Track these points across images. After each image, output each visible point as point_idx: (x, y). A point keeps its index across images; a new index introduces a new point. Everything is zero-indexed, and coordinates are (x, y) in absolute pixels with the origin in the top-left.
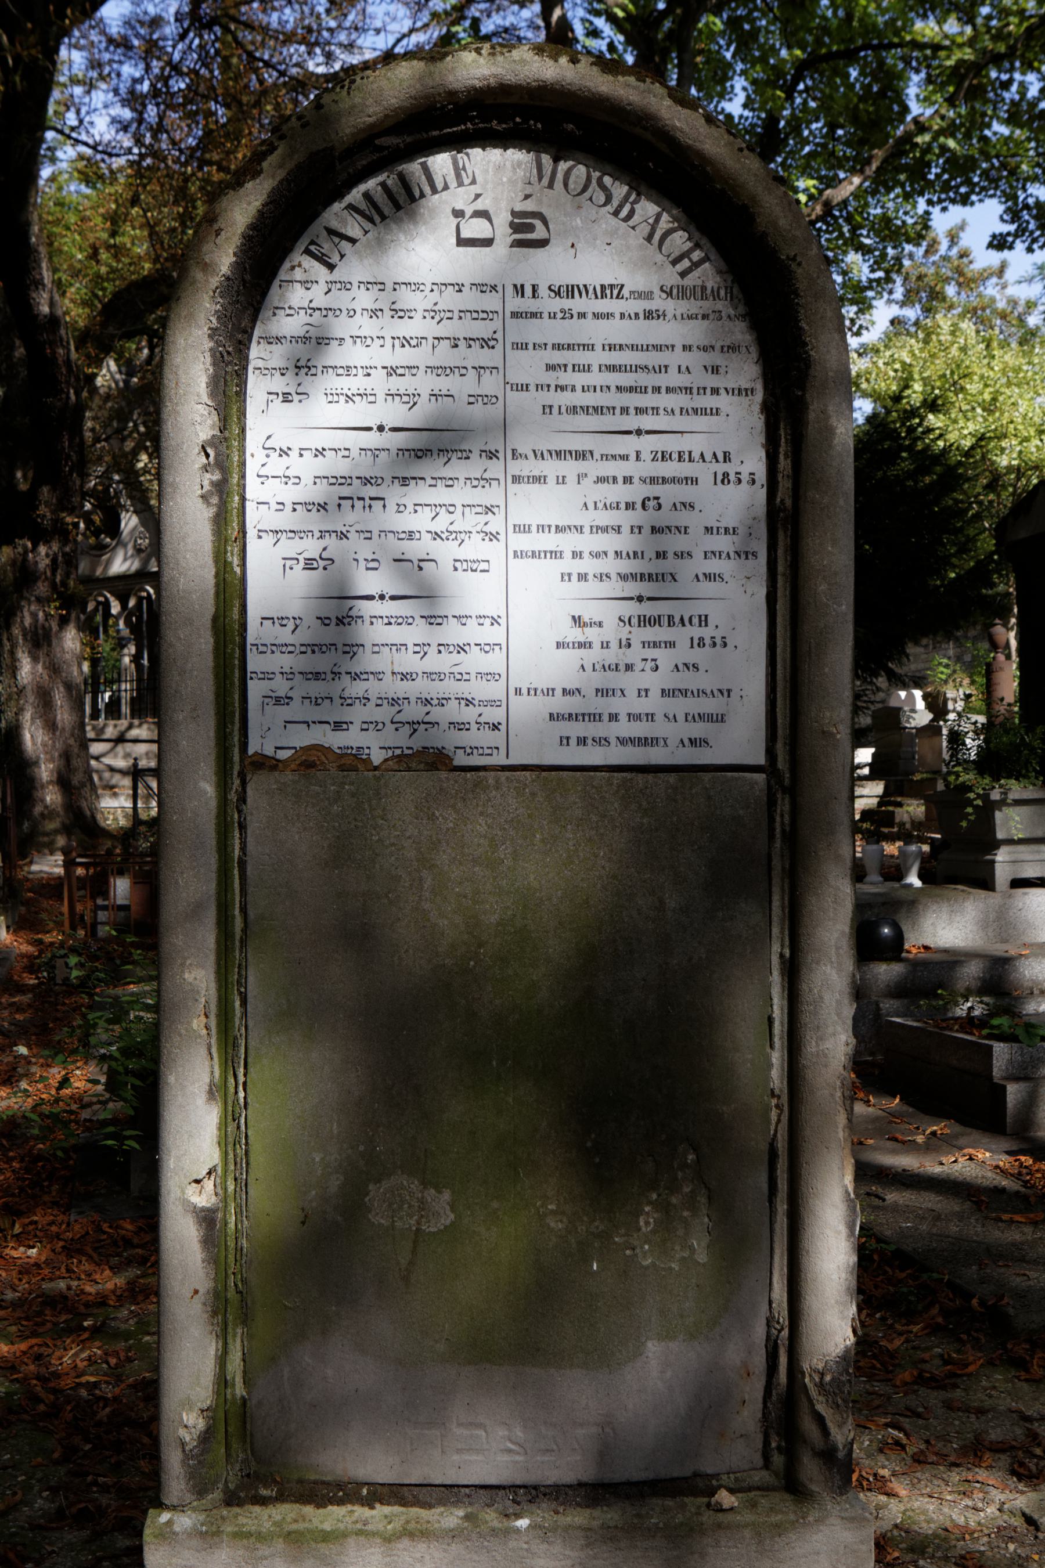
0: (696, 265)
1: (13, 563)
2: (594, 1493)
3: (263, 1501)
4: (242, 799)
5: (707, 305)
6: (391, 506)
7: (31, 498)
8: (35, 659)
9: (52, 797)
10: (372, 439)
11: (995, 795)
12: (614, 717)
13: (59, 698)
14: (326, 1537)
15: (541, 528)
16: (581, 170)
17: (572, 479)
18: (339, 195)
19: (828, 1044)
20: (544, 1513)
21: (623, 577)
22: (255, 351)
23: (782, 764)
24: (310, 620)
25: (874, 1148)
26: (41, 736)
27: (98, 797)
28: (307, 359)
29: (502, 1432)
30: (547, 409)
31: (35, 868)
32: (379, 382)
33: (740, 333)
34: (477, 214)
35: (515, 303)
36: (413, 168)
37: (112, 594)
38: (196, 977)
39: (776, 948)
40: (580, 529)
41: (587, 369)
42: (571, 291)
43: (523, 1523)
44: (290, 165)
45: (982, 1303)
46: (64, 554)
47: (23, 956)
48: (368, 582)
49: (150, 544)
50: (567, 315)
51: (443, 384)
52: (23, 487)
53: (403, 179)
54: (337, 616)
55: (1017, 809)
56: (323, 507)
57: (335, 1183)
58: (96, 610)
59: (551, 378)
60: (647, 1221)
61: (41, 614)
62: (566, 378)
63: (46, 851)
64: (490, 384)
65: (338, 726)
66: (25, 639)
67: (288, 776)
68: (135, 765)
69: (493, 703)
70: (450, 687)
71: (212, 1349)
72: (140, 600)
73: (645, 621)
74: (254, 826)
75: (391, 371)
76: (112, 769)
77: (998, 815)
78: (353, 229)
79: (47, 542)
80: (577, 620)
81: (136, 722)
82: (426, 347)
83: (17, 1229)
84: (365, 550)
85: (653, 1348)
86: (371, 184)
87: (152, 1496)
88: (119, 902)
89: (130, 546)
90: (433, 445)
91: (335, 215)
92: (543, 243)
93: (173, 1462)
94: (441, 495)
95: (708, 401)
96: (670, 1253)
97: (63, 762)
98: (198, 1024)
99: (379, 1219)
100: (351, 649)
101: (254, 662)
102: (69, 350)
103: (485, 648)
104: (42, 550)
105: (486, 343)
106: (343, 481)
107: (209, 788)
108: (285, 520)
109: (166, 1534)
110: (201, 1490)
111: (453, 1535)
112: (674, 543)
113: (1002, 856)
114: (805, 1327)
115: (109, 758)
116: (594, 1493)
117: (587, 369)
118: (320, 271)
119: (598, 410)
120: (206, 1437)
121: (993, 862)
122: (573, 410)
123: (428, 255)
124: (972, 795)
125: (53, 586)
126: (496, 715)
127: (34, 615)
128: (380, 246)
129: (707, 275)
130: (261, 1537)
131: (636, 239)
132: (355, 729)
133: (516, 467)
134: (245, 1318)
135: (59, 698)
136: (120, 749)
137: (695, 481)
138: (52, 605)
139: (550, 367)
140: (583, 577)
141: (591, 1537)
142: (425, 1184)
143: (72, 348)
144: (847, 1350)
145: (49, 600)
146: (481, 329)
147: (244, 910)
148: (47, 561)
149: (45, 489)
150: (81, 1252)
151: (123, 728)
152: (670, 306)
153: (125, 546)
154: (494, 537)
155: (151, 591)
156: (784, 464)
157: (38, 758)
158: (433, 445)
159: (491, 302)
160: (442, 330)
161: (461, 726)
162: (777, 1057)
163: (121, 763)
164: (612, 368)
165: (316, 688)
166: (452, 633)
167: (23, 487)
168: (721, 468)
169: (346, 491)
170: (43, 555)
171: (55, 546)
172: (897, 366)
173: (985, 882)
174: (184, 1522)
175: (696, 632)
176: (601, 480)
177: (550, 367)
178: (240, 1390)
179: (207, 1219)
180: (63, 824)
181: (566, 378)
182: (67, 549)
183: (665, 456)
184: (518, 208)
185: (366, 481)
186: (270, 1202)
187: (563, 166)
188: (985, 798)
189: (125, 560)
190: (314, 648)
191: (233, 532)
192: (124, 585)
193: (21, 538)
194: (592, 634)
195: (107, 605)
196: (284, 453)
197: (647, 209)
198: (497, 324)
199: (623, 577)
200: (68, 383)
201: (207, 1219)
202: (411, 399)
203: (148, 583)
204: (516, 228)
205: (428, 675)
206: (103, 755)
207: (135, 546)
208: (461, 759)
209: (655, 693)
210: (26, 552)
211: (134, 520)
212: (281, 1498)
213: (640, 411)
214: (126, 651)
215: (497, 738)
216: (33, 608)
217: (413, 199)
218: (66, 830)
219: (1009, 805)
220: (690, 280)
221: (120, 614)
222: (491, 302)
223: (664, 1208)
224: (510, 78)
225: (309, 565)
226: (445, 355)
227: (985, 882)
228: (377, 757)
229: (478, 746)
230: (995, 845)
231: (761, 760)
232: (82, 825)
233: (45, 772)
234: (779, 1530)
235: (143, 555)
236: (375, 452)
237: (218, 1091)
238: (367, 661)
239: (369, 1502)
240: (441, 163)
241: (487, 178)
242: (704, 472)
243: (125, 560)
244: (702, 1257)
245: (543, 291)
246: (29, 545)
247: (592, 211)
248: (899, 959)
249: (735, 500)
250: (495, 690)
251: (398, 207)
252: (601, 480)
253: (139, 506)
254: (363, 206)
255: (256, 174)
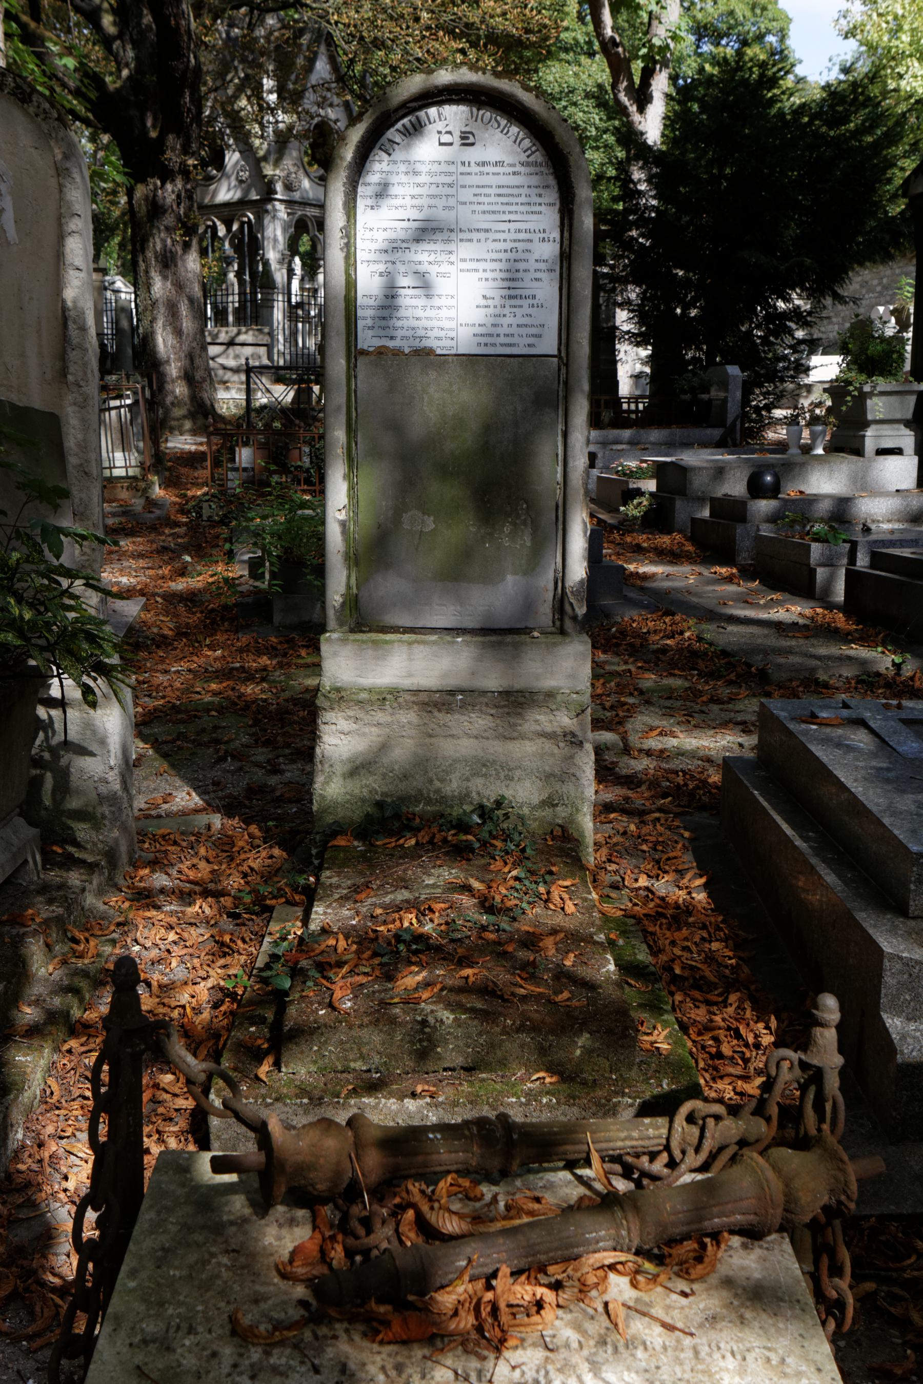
0: (533, 153)
1: (146, 198)
2: (484, 631)
3: (364, 632)
4: (356, 366)
5: (538, 169)
6: (413, 250)
7: (160, 145)
8: (165, 278)
9: (180, 390)
10: (405, 224)
11: (867, 388)
12: (498, 335)
13: (184, 309)
14: (386, 642)
15: (471, 260)
16: (488, 114)
17: (483, 240)
18: (392, 125)
19: (577, 463)
20: (468, 638)
21: (503, 280)
22: (360, 189)
23: (563, 354)
24: (381, 296)
25: (731, 607)
26: (171, 340)
27: (215, 390)
28: (382, 192)
29: (452, 608)
30: (474, 212)
31: (170, 445)
32: (408, 201)
33: (551, 181)
34: (447, 132)
35: (462, 169)
36: (422, 114)
37: (219, 219)
38: (339, 435)
39: (560, 427)
40: (486, 260)
41: (489, 195)
42: (484, 164)
43: (459, 639)
44: (374, 117)
45: (757, 669)
46: (187, 191)
47: (175, 504)
48: (403, 281)
49: (250, 176)
50: (482, 173)
51: (432, 202)
52: (153, 134)
53: (417, 118)
54: (389, 299)
55: (884, 398)
56: (386, 251)
57: (390, 513)
58: (206, 232)
59: (475, 199)
60: (507, 529)
61: (169, 241)
62: (481, 199)
63: (177, 433)
64: (452, 202)
65: (392, 338)
66: (157, 261)
67: (373, 358)
68: (247, 364)
69: (451, 329)
70: (435, 323)
71: (345, 573)
72: (242, 224)
73: (511, 297)
74: (360, 377)
75: (413, 197)
76: (224, 368)
77: (869, 402)
78: (398, 140)
79: (173, 181)
80: (484, 297)
81: (244, 329)
82: (426, 187)
83: (208, 642)
84: (402, 268)
85: (509, 578)
86: (405, 121)
87: (322, 628)
88: (244, 465)
89: (233, 178)
90: (427, 231)
91: (391, 133)
92: (472, 144)
93: (331, 613)
94: (432, 246)
95: (537, 208)
96: (514, 543)
97: (188, 362)
98: (339, 451)
99: (406, 527)
100: (396, 308)
101: (360, 313)
102: (189, 20)
103: (449, 308)
104: (169, 187)
105: (450, 185)
106: (394, 241)
107: (343, 362)
108: (372, 257)
109: (329, 640)
110: (341, 624)
111: (434, 643)
112: (522, 266)
113: (870, 432)
114: (567, 571)
115: (224, 359)
116: (484, 631)
117: (489, 195)
118: (384, 155)
119: (494, 212)
120: (343, 605)
121: (864, 436)
122: (484, 212)
123: (427, 151)
124: (851, 388)
125: (179, 219)
126: (453, 334)
127: (163, 241)
128: (408, 146)
129: (538, 157)
130: (363, 642)
131: (510, 142)
132: (398, 339)
133: (461, 236)
134: (357, 564)
135: (184, 309)
136: (231, 351)
137: (531, 241)
138: (178, 233)
139: (475, 195)
140: (487, 279)
141: (484, 645)
142: (424, 513)
143: (192, 19)
144: (583, 579)
145: (175, 229)
146: (448, 180)
147: (356, 409)
148: (173, 197)
149: (171, 137)
150: (248, 651)
151: (233, 334)
152: (522, 169)
153: (229, 177)
154: (452, 263)
155: (252, 217)
156: (566, 234)
157: (169, 358)
158: (427, 231)
159: (452, 168)
160: (433, 180)
161: (439, 339)
162: (560, 469)
163: (231, 363)
164: (499, 195)
165: (383, 323)
166: (436, 302)
167: (153, 134)
168: (542, 235)
169: (395, 245)
170: (169, 192)
171: (179, 184)
172: (890, 18)
173: (858, 451)
174: (335, 636)
175: (531, 301)
176: (494, 240)
177: (475, 195)
178: (355, 591)
179: (343, 524)
180: (189, 410)
181: (481, 199)
182: (189, 187)
183: (520, 231)
184: (464, 129)
185: (403, 241)
186: (366, 518)
187: (481, 112)
188: (860, 390)
189: (229, 190)
190: (383, 307)
191: (352, 262)
192: (228, 212)
193: (152, 177)
194: (490, 302)
195: (214, 228)
196: (371, 230)
197: (514, 130)
198: (454, 177)
199: (503, 280)
200: (189, 48)
201: (343, 524)
202: (420, 208)
203: (248, 210)
204: (462, 138)
205: (426, 318)
206: (218, 356)
207: (237, 178)
208: (439, 352)
209: (514, 326)
210: (156, 189)
211: (237, 155)
212: (370, 631)
213: (510, 212)
214: (230, 268)
215: (453, 343)
216: (162, 235)
217: (421, 126)
218: (192, 415)
219: (876, 395)
220: (532, 159)
221: (225, 236)
222: (452, 168)
223: (514, 524)
224: (459, 80)
225: (381, 275)
226: (434, 190)
227: (858, 451)
228: (407, 351)
229: (441, 346)
230: (866, 424)
231: (556, 353)
232: (202, 412)
233: (173, 370)
234: (555, 644)
235: (243, 185)
236: (406, 229)
237: (347, 477)
238: (402, 313)
239: (404, 633)
240: (433, 111)
241: (449, 118)
242: (536, 237)
243: (229, 190)
244: (528, 544)
245: (472, 164)
246: (159, 183)
247: (491, 131)
248: (775, 497)
249: (549, 250)
250: (452, 324)
251: (416, 130)
252: (494, 240)
253: (241, 145)
254: (402, 129)
255: (361, 121)
